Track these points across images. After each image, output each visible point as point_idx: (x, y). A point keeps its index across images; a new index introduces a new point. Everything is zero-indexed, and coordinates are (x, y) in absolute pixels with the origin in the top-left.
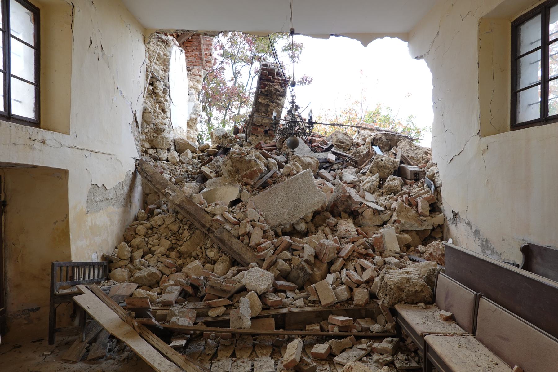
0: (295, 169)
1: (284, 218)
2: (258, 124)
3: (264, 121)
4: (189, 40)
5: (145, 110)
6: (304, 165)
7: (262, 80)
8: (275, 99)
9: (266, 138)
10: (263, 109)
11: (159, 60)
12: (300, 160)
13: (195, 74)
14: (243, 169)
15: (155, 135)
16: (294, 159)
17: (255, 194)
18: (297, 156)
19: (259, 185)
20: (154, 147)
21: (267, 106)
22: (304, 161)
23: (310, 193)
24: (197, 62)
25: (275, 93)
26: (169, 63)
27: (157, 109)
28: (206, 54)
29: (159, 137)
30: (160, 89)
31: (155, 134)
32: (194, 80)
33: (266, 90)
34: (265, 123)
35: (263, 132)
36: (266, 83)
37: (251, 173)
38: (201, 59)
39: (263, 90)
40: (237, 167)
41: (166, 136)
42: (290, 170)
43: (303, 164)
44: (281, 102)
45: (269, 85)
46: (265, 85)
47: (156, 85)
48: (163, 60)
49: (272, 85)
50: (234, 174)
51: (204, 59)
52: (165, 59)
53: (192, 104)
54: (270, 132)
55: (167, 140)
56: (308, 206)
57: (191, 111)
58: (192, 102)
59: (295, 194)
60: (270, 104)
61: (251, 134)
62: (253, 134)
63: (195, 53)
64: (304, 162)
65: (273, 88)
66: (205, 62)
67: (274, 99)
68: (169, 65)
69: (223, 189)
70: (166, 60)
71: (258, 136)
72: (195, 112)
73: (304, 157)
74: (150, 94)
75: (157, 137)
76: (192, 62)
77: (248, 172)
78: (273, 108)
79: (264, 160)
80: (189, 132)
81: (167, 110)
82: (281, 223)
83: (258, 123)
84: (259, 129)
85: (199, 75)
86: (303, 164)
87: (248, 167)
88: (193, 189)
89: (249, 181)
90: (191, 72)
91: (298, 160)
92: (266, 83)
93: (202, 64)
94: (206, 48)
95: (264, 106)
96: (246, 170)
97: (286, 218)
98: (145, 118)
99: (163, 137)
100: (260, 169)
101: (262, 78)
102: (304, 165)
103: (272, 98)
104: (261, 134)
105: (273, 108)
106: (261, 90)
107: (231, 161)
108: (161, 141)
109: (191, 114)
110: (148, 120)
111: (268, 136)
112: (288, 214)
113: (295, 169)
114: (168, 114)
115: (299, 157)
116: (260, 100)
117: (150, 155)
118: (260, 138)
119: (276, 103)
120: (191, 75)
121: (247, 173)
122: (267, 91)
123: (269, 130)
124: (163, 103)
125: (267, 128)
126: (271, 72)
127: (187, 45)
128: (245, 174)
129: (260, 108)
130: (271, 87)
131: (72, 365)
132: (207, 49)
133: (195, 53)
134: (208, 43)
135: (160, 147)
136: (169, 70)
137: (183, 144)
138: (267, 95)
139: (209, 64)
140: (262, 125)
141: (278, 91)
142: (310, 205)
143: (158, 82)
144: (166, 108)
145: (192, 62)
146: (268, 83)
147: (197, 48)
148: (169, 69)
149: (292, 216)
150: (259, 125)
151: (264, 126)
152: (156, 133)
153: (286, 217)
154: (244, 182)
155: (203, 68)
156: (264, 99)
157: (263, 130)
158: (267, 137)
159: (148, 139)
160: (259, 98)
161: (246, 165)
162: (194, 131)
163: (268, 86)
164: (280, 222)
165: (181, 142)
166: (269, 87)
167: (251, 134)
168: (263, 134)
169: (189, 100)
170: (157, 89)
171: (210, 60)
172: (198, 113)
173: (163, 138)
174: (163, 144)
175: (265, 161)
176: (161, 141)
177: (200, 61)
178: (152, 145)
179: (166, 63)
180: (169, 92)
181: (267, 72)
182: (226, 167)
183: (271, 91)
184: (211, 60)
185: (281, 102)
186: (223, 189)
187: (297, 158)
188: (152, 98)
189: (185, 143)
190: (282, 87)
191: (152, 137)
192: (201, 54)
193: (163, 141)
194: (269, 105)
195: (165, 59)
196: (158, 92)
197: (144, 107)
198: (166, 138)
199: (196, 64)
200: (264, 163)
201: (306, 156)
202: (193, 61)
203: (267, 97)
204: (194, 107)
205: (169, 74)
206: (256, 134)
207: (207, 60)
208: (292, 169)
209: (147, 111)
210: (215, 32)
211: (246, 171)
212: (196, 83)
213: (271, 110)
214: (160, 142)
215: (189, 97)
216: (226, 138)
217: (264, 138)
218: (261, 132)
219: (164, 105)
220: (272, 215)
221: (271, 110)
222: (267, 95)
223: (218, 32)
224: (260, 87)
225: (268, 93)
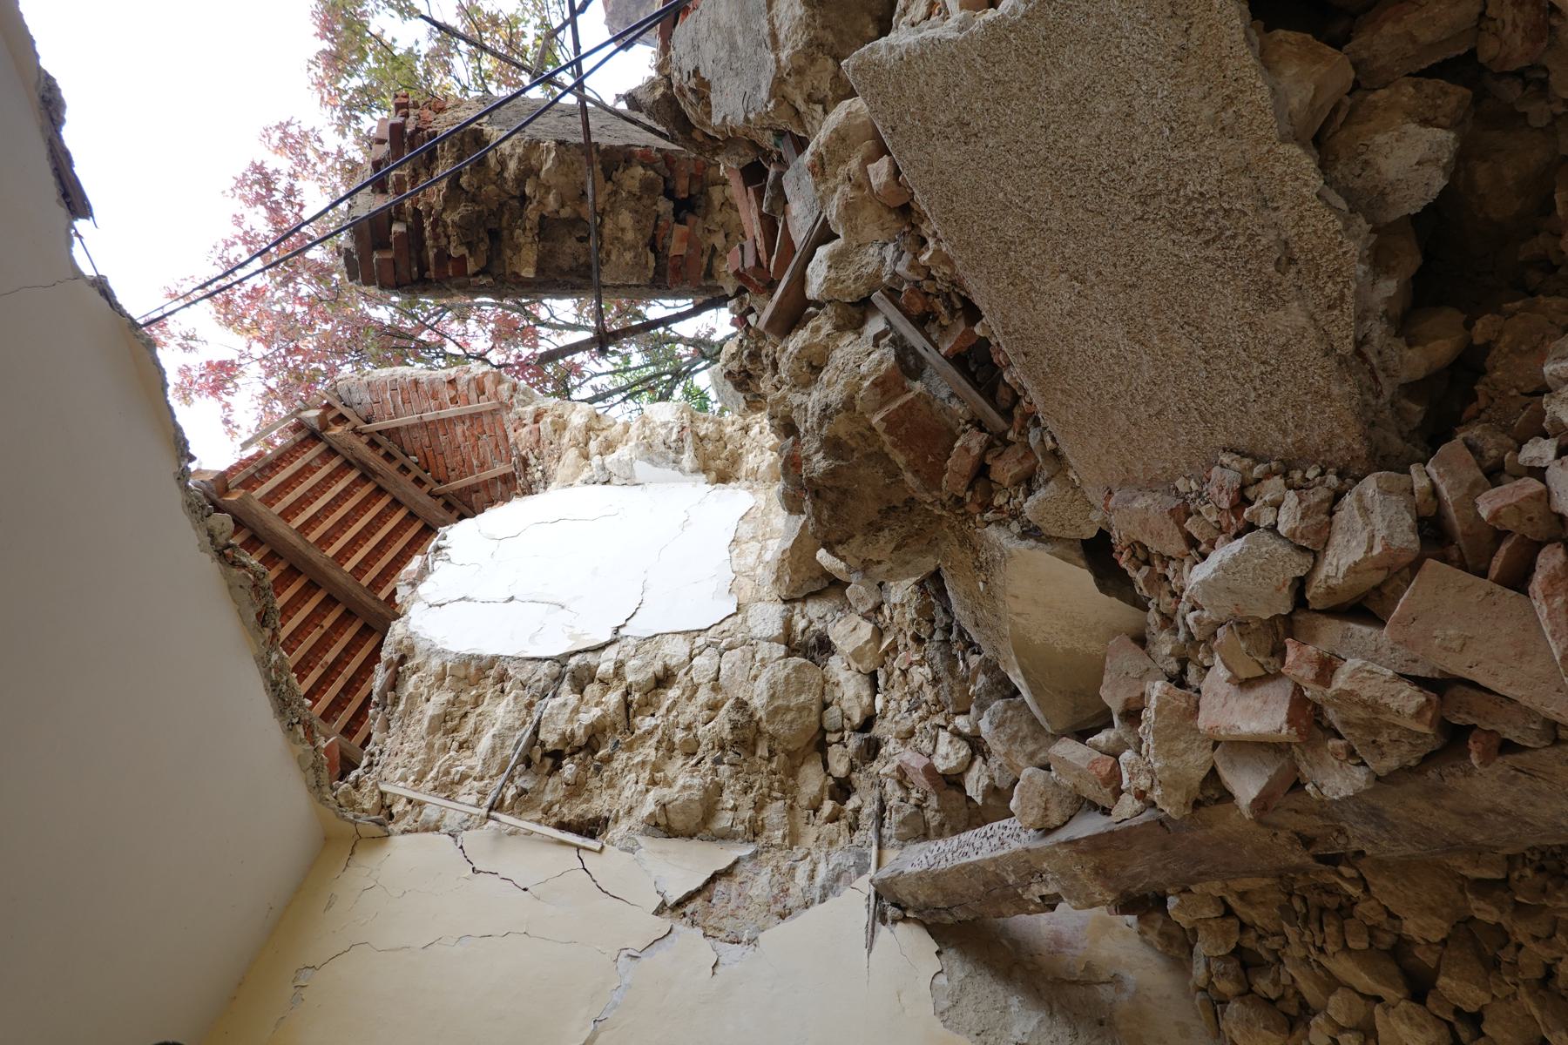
0: (854, 164)
1: (1301, 334)
2: (652, 264)
3: (630, 236)
4: (423, 461)
5: (657, 825)
6: (830, 38)
7: (427, 275)
8: (500, 187)
9: (717, 203)
10: (570, 245)
11: (462, 712)
12: (799, 71)
13: (533, 439)
14: (887, 486)
15: (762, 751)
16: (797, 112)
17: (1055, 455)
18: (772, 94)
19: (989, 409)
20: (818, 738)
21: (546, 228)
22: (801, 39)
23: (1069, 86)
24: (492, 429)
25: (473, 199)
26: (471, 657)
27: (657, 726)
28: (453, 400)
29: (770, 728)
30: (571, 720)
31: (759, 753)
32: (555, 442)
33: (463, 250)
34: (636, 230)
35: (685, 228)
36: (431, 254)
37: (904, 443)
38: (476, 417)
39: (471, 267)
40: (875, 517)
41: (765, 696)
42: (869, 212)
43: (821, 46)
44: (511, 156)
45: (436, 238)
46: (443, 256)
47: (556, 744)
48: (461, 685)
49: (434, 225)
50: (919, 520)
51: (474, 407)
52: (459, 679)
53: (642, 469)
54: (682, 187)
55: (780, 688)
56: (1207, 112)
57: (668, 471)
58: (632, 469)
59: (1067, 211)
60: (532, 212)
61: (709, 283)
62: (709, 274)
63: (460, 438)
64: (809, 44)
65: (450, 217)
66: (485, 404)
67: (505, 197)
68: (480, 658)
69: (1018, 614)
70: (462, 674)
71: (714, 248)
72: (672, 455)
73: (774, 36)
74: (598, 770)
75: (773, 738)
76: (497, 446)
77: (900, 459)
78: (551, 197)
79: (817, 329)
80: (754, 472)
81: (658, 666)
82: (1342, 360)
83: (646, 266)
84: (676, 247)
85: (536, 421)
86: (821, 46)
87: (868, 456)
88: (1016, 747)
89: (959, 462)
90: (531, 456)
91: (799, 85)
92: (431, 254)
93: (493, 412)
94: (432, 403)
95: (549, 245)
96: (888, 474)
97: (1302, 320)
98: (693, 824)
99: (768, 714)
100: (874, 384)
101: (415, 277)
102: (830, 38)
103: (501, 205)
104: (699, 233)
105: (551, 197)
106: (476, 275)
107: (840, 542)
108: (789, 717)
109: (681, 470)
110: (697, 810)
111: (704, 192)
112: (1268, 295)
113: (854, 164)
114: (676, 651)
115: (779, 81)
116: (528, 273)
117: (852, 768)
118: (722, 235)
119: (520, 180)
120: (541, 453)
121: (908, 464)
122: (469, 245)
123: (669, 193)
124: (631, 686)
125: (664, 206)
126: (367, 233)
127: (441, 470)
128: (916, 473)
129: (565, 262)
130: (445, 226)
131: (1498, 506)
132: (435, 397)
133: (460, 438)
134: (414, 395)
135: (814, 718)
136: (498, 657)
137: (795, 571)
138: (494, 235)
139: (489, 384)
140: (654, 236)
141: (455, 178)
142: (1196, 92)
143: (541, 737)
144: (651, 670)
145: (497, 446)
146: (429, 243)
147: (441, 433)
148: (495, 659)
149: (1287, 261)
150: (651, 256)
151: (656, 226)
152: (755, 745)
153: (1292, 317)
154: (970, 487)
155: (509, 408)
156: (517, 248)
157: (680, 230)
158: (709, 201)
159: (781, 782)
160: (517, 275)
161: (861, 471)
162: (747, 441)
163: (443, 241)
164: (1332, 363)
165: (787, 579)
166: (448, 237)
167: (709, 283)
168: (696, 223)
169: (630, 481)
170: (573, 734)
171: (473, 385)
172: (674, 437)
173: (774, 713)
174: (802, 708)
175: (824, 324)
176: (789, 717)
177: (486, 420)
178: (812, 746)
179: (472, 670)
180: (586, 651)
181: (376, 256)
182: (879, 562)
183: (464, 226)
184: (469, 381)
185: (511, 156)
186: (1018, 614)
187: (789, 89)
188: (608, 759)
189: (790, 563)
190: (432, 157)
191: (774, 766)
192: (461, 419)
193: (788, 709)
194: (542, 217)
195: (459, 679)
196: (582, 731)
197: (645, 833)
198: (772, 696)
199: (499, 432)
200: (840, 329)
201: (766, 29)
202: (492, 446)
203: (505, 233)
204: (651, 461)
205: (514, 659)
206: (705, 260)
207: (473, 396)
208: (859, 187)
209: (662, 821)
210: (230, 587)
211: (894, 474)
212: (567, 435)
213: (563, 206)
214: (792, 721)
215: (614, 479)
216: (749, 376)
217: (719, 218)
218: (689, 239)
219: (637, 684)
220: (1254, 409)
221: (563, 206)
222: (494, 235)
223: (226, 576)
224: (462, 280)
225: (483, 234)
